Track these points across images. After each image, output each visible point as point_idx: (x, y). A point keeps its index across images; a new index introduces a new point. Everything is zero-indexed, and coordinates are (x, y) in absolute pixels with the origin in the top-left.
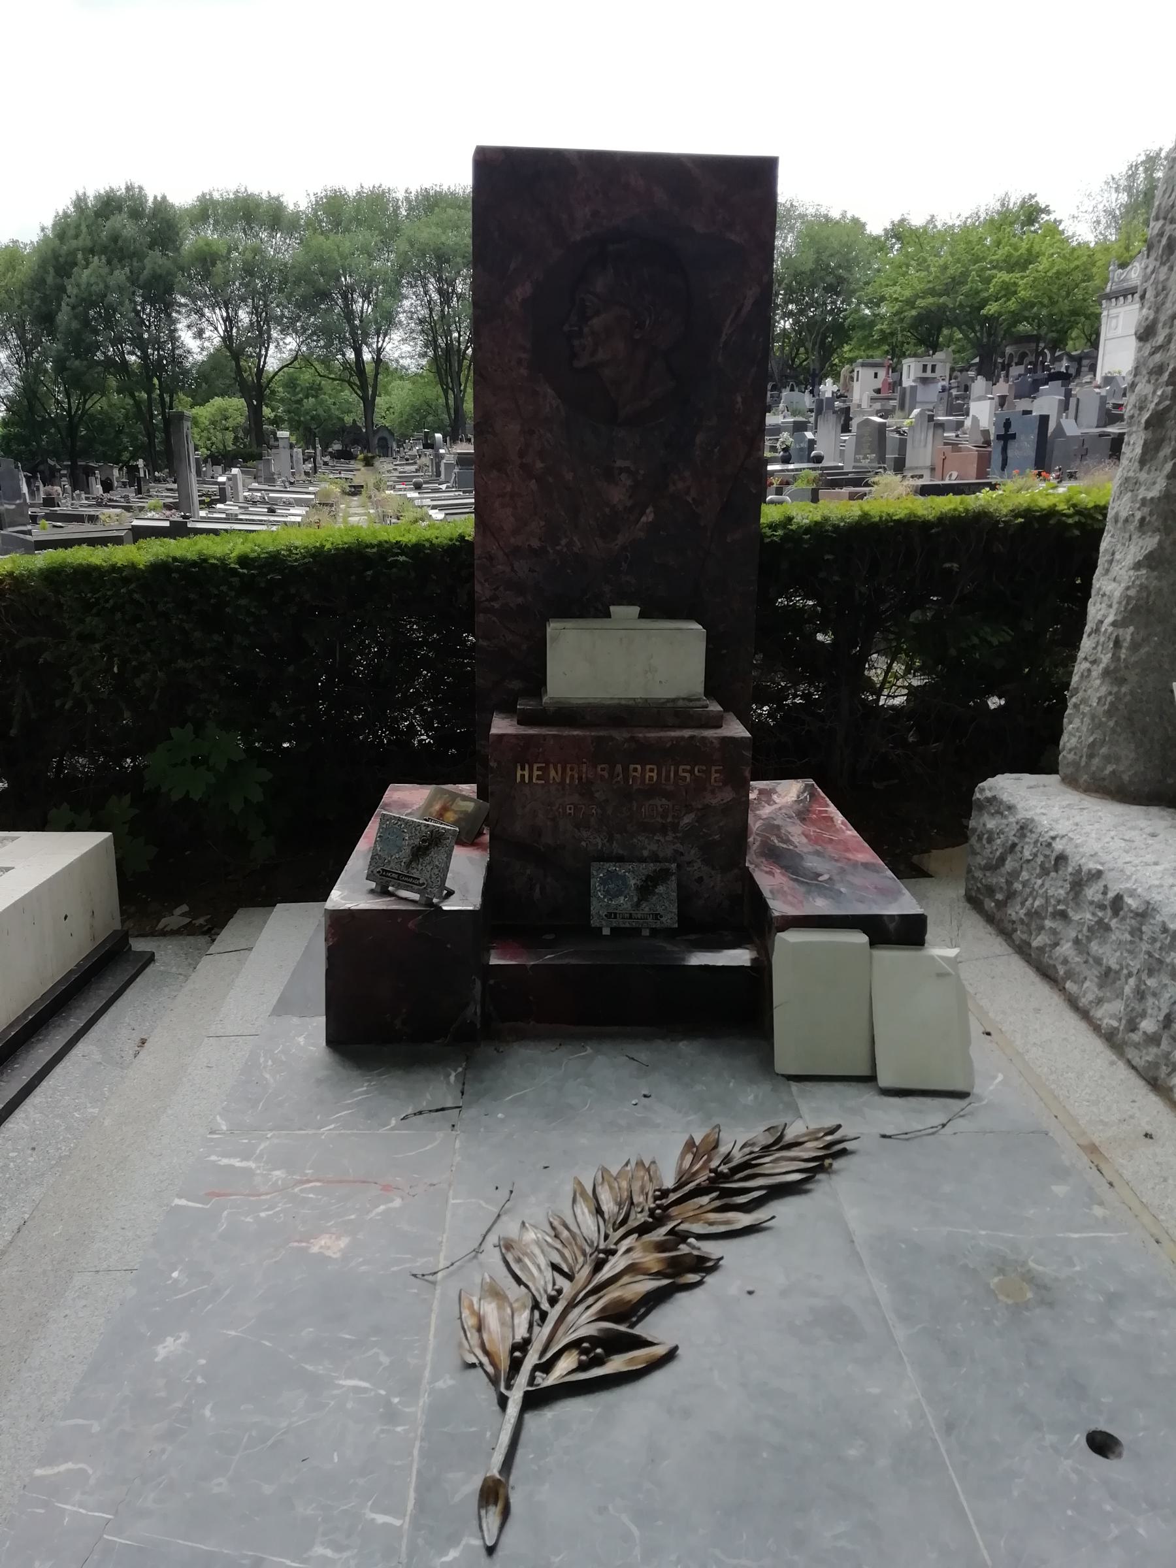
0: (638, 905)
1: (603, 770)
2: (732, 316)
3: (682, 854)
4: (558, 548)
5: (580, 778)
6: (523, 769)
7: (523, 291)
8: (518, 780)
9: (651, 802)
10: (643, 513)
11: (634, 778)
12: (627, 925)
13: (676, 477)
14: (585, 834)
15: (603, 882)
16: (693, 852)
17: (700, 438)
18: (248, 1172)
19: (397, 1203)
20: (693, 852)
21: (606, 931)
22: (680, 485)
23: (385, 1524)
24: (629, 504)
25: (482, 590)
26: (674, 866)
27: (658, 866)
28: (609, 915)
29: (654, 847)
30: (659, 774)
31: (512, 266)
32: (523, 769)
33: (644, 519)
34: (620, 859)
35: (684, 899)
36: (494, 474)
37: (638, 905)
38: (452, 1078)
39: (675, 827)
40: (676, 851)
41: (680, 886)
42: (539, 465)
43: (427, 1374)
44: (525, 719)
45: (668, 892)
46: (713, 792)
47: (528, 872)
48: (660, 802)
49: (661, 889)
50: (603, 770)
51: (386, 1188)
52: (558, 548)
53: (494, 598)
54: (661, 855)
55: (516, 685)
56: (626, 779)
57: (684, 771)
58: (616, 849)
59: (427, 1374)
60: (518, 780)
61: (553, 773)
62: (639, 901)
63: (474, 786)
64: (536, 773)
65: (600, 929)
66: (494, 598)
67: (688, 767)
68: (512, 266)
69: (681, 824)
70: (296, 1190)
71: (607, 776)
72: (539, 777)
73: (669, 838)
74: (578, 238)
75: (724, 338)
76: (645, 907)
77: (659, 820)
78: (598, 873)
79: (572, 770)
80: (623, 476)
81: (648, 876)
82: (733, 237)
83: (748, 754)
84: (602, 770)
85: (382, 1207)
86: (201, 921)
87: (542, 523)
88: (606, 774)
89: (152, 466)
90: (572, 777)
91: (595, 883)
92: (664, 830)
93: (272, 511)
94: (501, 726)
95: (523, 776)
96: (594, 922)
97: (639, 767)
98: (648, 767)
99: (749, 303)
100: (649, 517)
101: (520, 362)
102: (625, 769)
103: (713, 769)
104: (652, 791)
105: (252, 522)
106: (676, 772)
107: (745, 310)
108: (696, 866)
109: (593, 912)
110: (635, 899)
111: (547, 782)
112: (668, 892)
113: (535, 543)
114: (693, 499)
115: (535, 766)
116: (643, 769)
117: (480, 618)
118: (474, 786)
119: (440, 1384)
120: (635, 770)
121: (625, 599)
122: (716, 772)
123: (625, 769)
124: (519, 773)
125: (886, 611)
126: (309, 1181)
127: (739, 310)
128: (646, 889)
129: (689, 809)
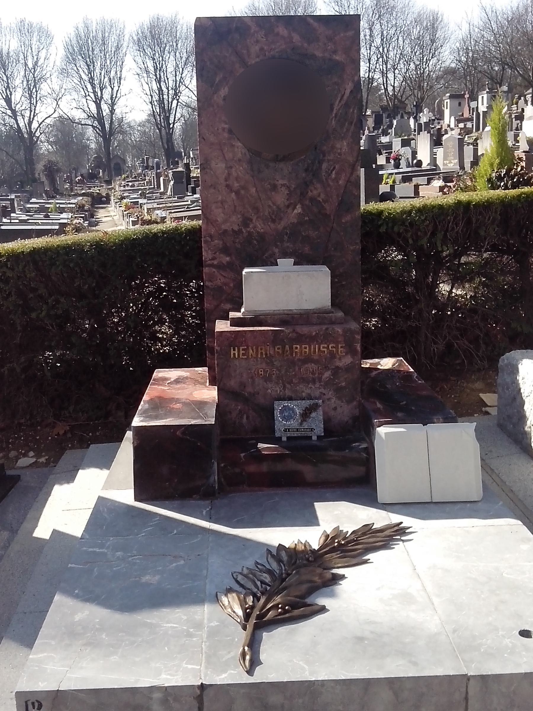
0: (301, 424)
1: (278, 349)
2: (339, 99)
3: (324, 394)
4: (248, 229)
5: (266, 354)
6: (234, 350)
7: (224, 91)
8: (232, 356)
9: (306, 366)
10: (294, 208)
11: (296, 352)
12: (295, 435)
13: (312, 188)
14: (270, 385)
15: (281, 412)
16: (330, 393)
17: (324, 166)
18: (105, 554)
19: (182, 562)
20: (330, 393)
21: (284, 439)
22: (315, 192)
23: (192, 668)
24: (287, 203)
25: (206, 255)
26: (320, 401)
27: (312, 402)
28: (285, 430)
29: (308, 391)
30: (310, 349)
31: (217, 79)
32: (234, 350)
33: (296, 211)
34: (290, 399)
35: (327, 421)
36: (212, 191)
37: (301, 424)
38: (204, 513)
39: (320, 380)
40: (321, 393)
41: (325, 413)
42: (236, 185)
43: (206, 621)
44: (235, 322)
45: (318, 417)
46: (340, 359)
47: (239, 407)
48: (312, 366)
49: (313, 415)
50: (278, 349)
51: (175, 557)
52: (248, 229)
53: (214, 259)
54: (312, 395)
55: (228, 306)
56: (292, 355)
57: (323, 348)
58: (288, 393)
59: (206, 621)
60: (232, 356)
61: (251, 351)
62: (302, 421)
63: (206, 369)
64: (242, 352)
65: (281, 438)
66: (214, 259)
67: (326, 346)
68: (217, 79)
69: (323, 377)
70: (130, 559)
71: (281, 352)
72: (243, 354)
73: (317, 385)
74: (253, 62)
75: (335, 112)
76: (305, 425)
77: (311, 376)
78: (278, 406)
79: (261, 349)
80: (283, 189)
81: (307, 408)
82: (337, 58)
83: (358, 337)
84: (278, 349)
85: (174, 565)
86: (42, 460)
87: (239, 216)
88: (280, 351)
89: (128, 208)
90: (262, 353)
91: (277, 413)
92: (314, 381)
93: (47, 216)
94: (222, 326)
95: (234, 354)
96: (277, 434)
97: (298, 346)
98: (303, 346)
99: (348, 92)
100: (299, 209)
101: (224, 129)
102: (291, 348)
103: (340, 346)
104: (308, 360)
105: (36, 224)
106: (319, 349)
107: (345, 97)
108: (333, 401)
109: (276, 429)
110: (300, 421)
111: (248, 357)
112: (318, 417)
113: (236, 228)
114: (322, 199)
115: (241, 348)
116: (301, 347)
117: (206, 270)
118: (206, 369)
119: (212, 624)
120: (297, 348)
121: (285, 255)
122: (341, 347)
123: (291, 348)
124: (232, 352)
125: (446, 257)
126: (134, 556)
127: (343, 96)
128: (306, 414)
129: (326, 368)
